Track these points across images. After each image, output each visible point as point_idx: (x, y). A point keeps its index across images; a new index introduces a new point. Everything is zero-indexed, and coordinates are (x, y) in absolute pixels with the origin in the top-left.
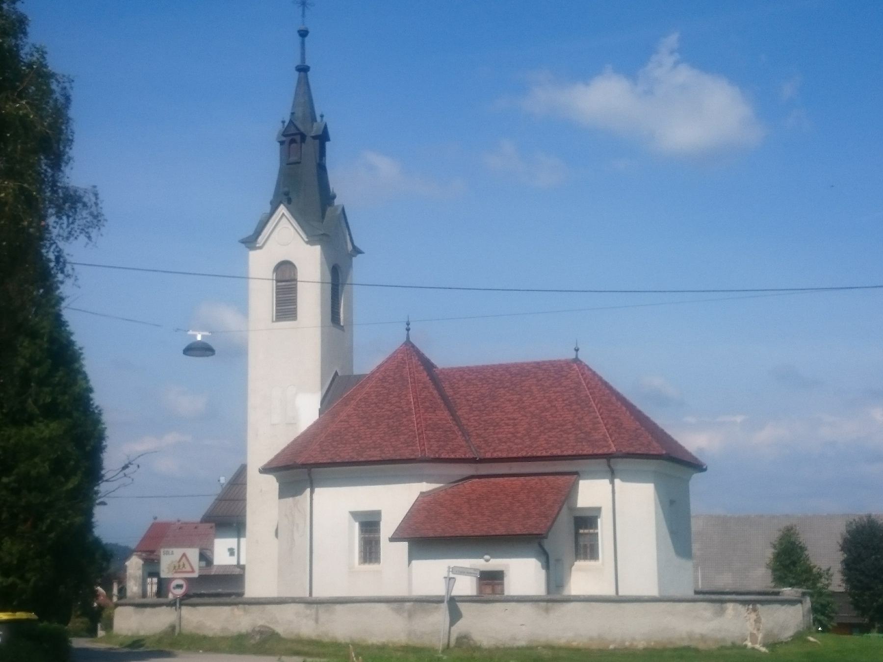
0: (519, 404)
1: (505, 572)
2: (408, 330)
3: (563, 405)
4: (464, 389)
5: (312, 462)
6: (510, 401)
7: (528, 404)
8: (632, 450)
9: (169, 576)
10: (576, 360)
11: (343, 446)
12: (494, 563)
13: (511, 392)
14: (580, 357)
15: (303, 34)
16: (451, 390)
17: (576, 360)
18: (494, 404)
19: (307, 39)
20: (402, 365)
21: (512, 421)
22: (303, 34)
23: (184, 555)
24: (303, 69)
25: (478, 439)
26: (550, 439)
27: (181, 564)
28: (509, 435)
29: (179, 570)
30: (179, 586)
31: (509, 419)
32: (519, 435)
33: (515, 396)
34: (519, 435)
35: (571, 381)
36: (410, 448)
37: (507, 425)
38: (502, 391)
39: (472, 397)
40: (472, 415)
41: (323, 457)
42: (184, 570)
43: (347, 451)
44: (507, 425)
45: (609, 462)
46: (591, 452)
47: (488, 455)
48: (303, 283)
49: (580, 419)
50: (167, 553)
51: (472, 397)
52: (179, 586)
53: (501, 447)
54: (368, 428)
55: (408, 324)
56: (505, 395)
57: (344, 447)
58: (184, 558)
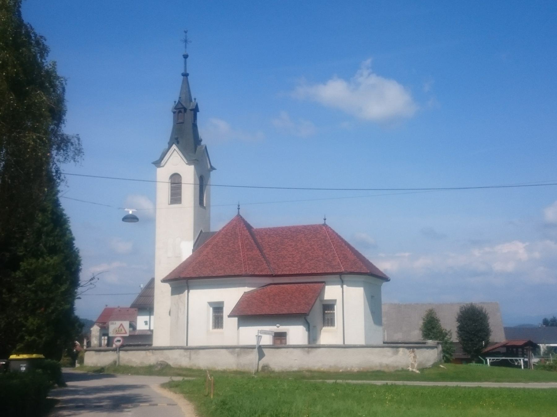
2: (239, 209)
6: (291, 245)
8: (352, 270)
9: (114, 335)
10: (325, 225)
11: (205, 268)
12: (282, 328)
18: (283, 247)
22: (186, 57)
23: (121, 325)
26: (311, 265)
27: (120, 329)
29: (119, 332)
30: (119, 341)
37: (289, 257)
38: (286, 240)
39: (271, 243)
42: (121, 332)
44: (289, 257)
46: (331, 272)
49: (326, 255)
50: (113, 324)
52: (119, 341)
55: (239, 206)
58: (121, 327)
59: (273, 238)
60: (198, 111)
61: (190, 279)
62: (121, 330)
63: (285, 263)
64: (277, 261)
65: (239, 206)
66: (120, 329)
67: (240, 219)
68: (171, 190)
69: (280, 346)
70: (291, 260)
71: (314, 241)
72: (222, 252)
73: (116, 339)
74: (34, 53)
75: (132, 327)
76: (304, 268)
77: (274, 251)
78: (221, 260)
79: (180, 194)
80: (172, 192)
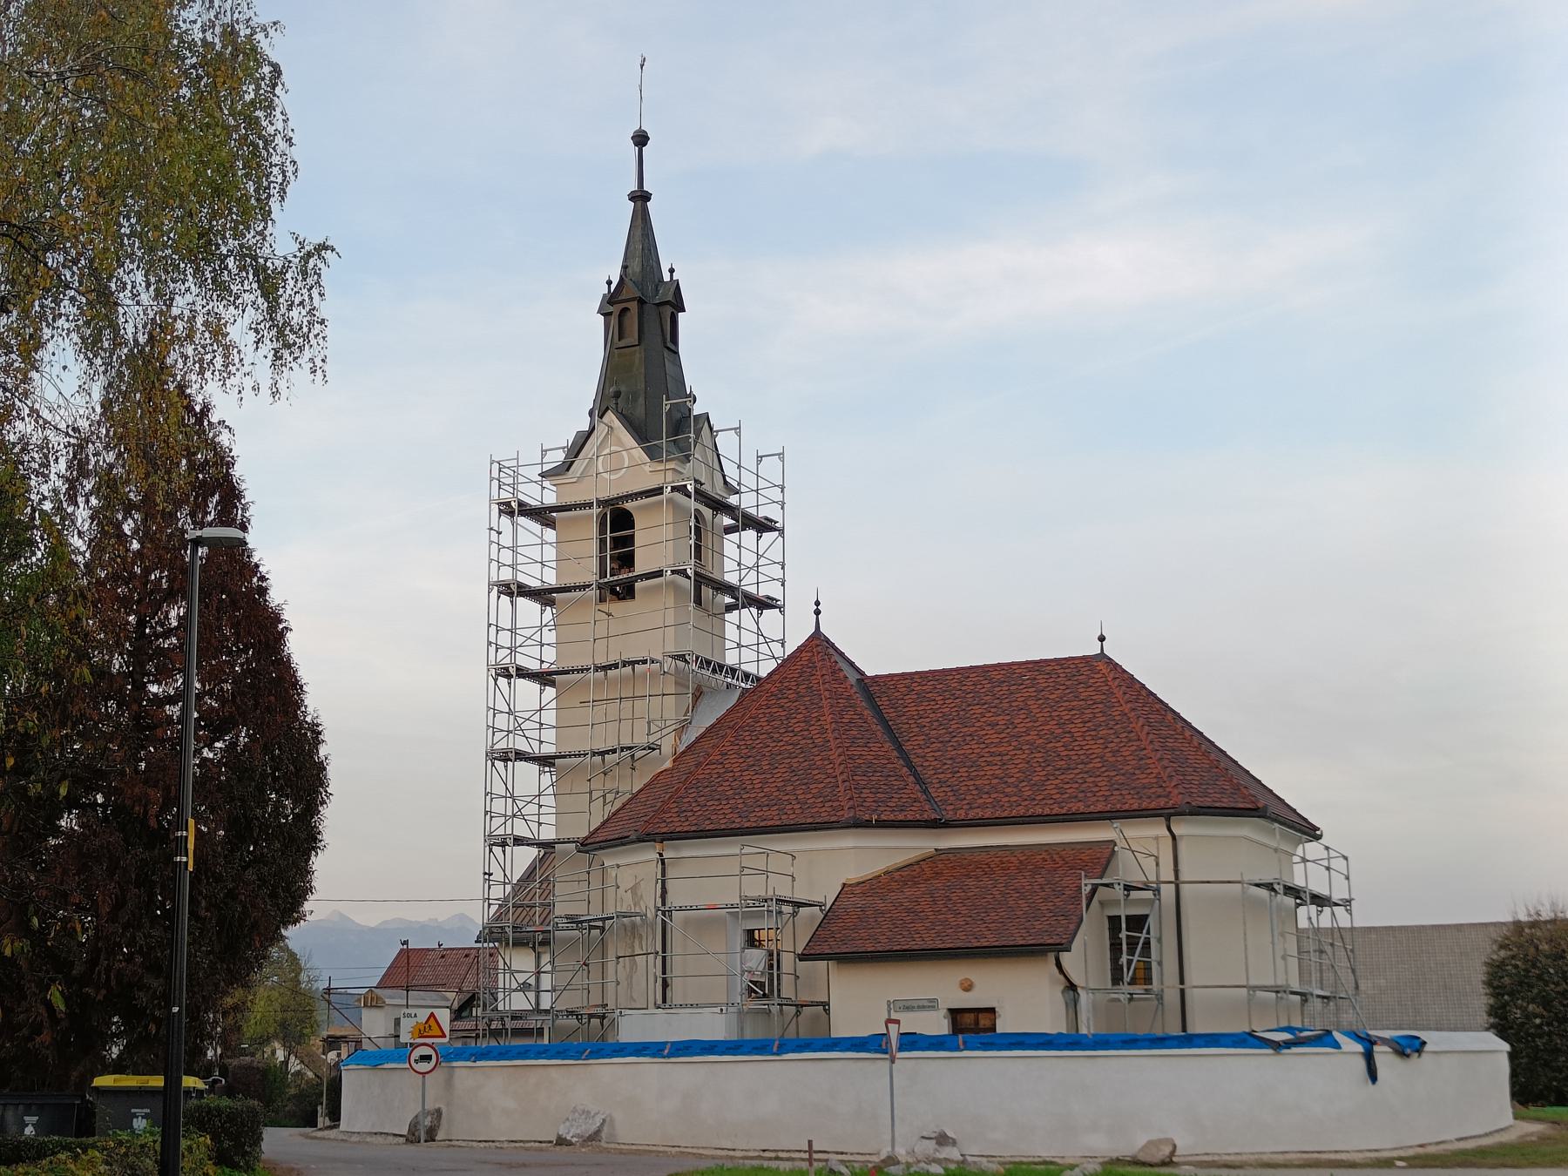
0: (1009, 730)
1: (996, 1010)
2: (817, 612)
6: (993, 725)
7: (1024, 729)
8: (1208, 802)
10: (1102, 655)
11: (716, 803)
13: (993, 710)
15: (641, 139)
20: (809, 670)
22: (641, 139)
23: (432, 1015)
25: (942, 789)
26: (1067, 786)
29: (425, 1034)
31: (992, 754)
33: (1001, 717)
37: (989, 763)
38: (978, 710)
39: (928, 720)
40: (929, 750)
42: (431, 1033)
44: (989, 763)
45: (1168, 820)
46: (1135, 806)
47: (961, 814)
48: (601, 970)
49: (1114, 753)
51: (928, 720)
55: (817, 603)
59: (932, 703)
64: (950, 776)
65: (819, 604)
67: (818, 644)
69: (1276, 934)
70: (997, 772)
74: (89, 1105)
77: (939, 745)
78: (768, 776)
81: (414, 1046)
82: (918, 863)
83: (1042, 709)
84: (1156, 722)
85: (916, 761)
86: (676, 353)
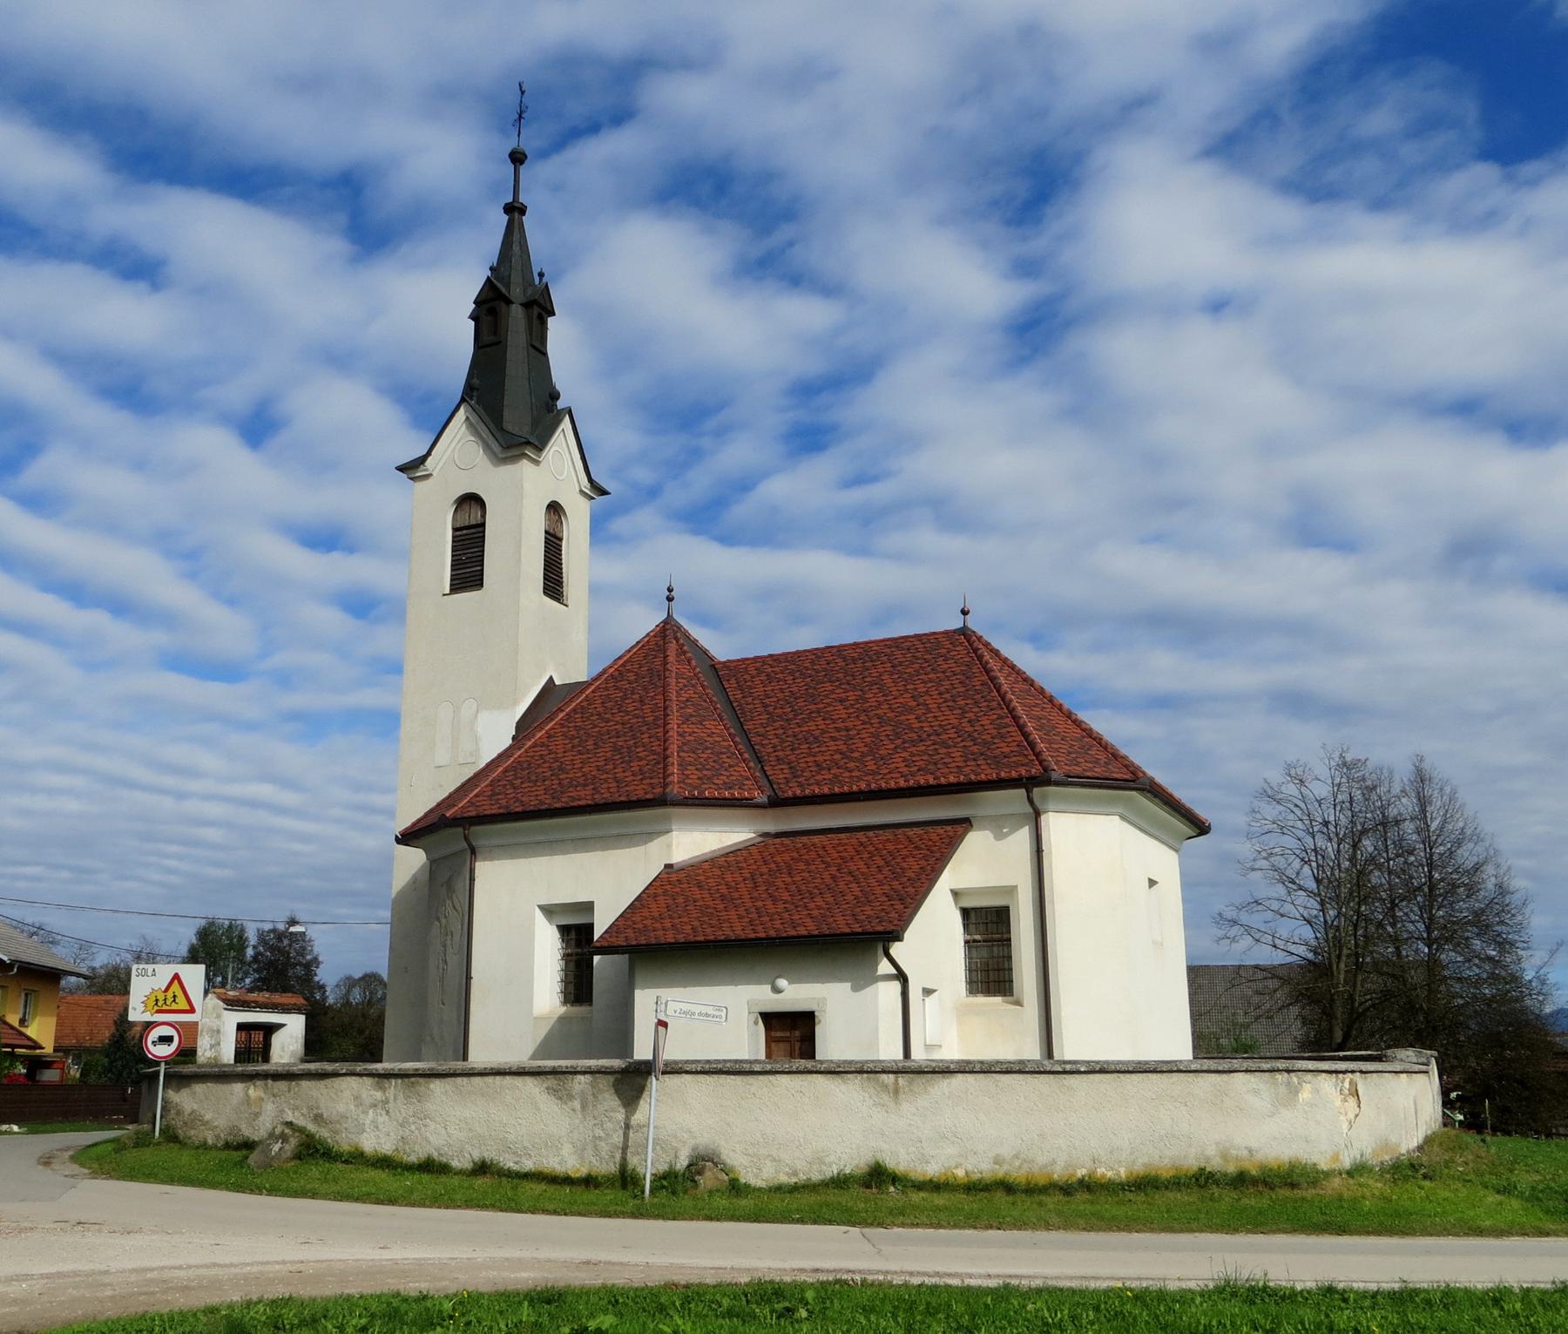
1: (816, 1014)
2: (670, 599)
3: (941, 701)
4: (762, 689)
5: (473, 814)
9: (147, 1017)
11: (531, 785)
12: (794, 994)
14: (970, 625)
16: (739, 692)
17: (964, 632)
18: (813, 707)
19: (522, 169)
21: (843, 733)
23: (176, 977)
24: (515, 210)
27: (170, 994)
28: (837, 757)
29: (165, 1007)
30: (166, 1040)
31: (838, 730)
32: (856, 755)
34: (856, 755)
35: (955, 662)
36: (648, 781)
37: (833, 739)
41: (493, 805)
42: (174, 1007)
43: (535, 793)
44: (833, 739)
50: (144, 974)
52: (166, 1040)
53: (819, 777)
54: (580, 753)
55: (670, 590)
56: (832, 692)
57: (532, 787)
58: (176, 987)
60: (552, 313)
61: (475, 824)
62: (175, 996)
63: (820, 758)
66: (170, 994)
68: (1009, 940)
71: (924, 682)
72: (597, 729)
73: (155, 1034)
75: (1420, 1040)
76: (886, 771)
79: (480, 560)
80: (456, 555)
81: (149, 1026)
82: (746, 848)
83: (897, 683)
84: (1020, 691)
85: (755, 739)
86: (545, 354)
